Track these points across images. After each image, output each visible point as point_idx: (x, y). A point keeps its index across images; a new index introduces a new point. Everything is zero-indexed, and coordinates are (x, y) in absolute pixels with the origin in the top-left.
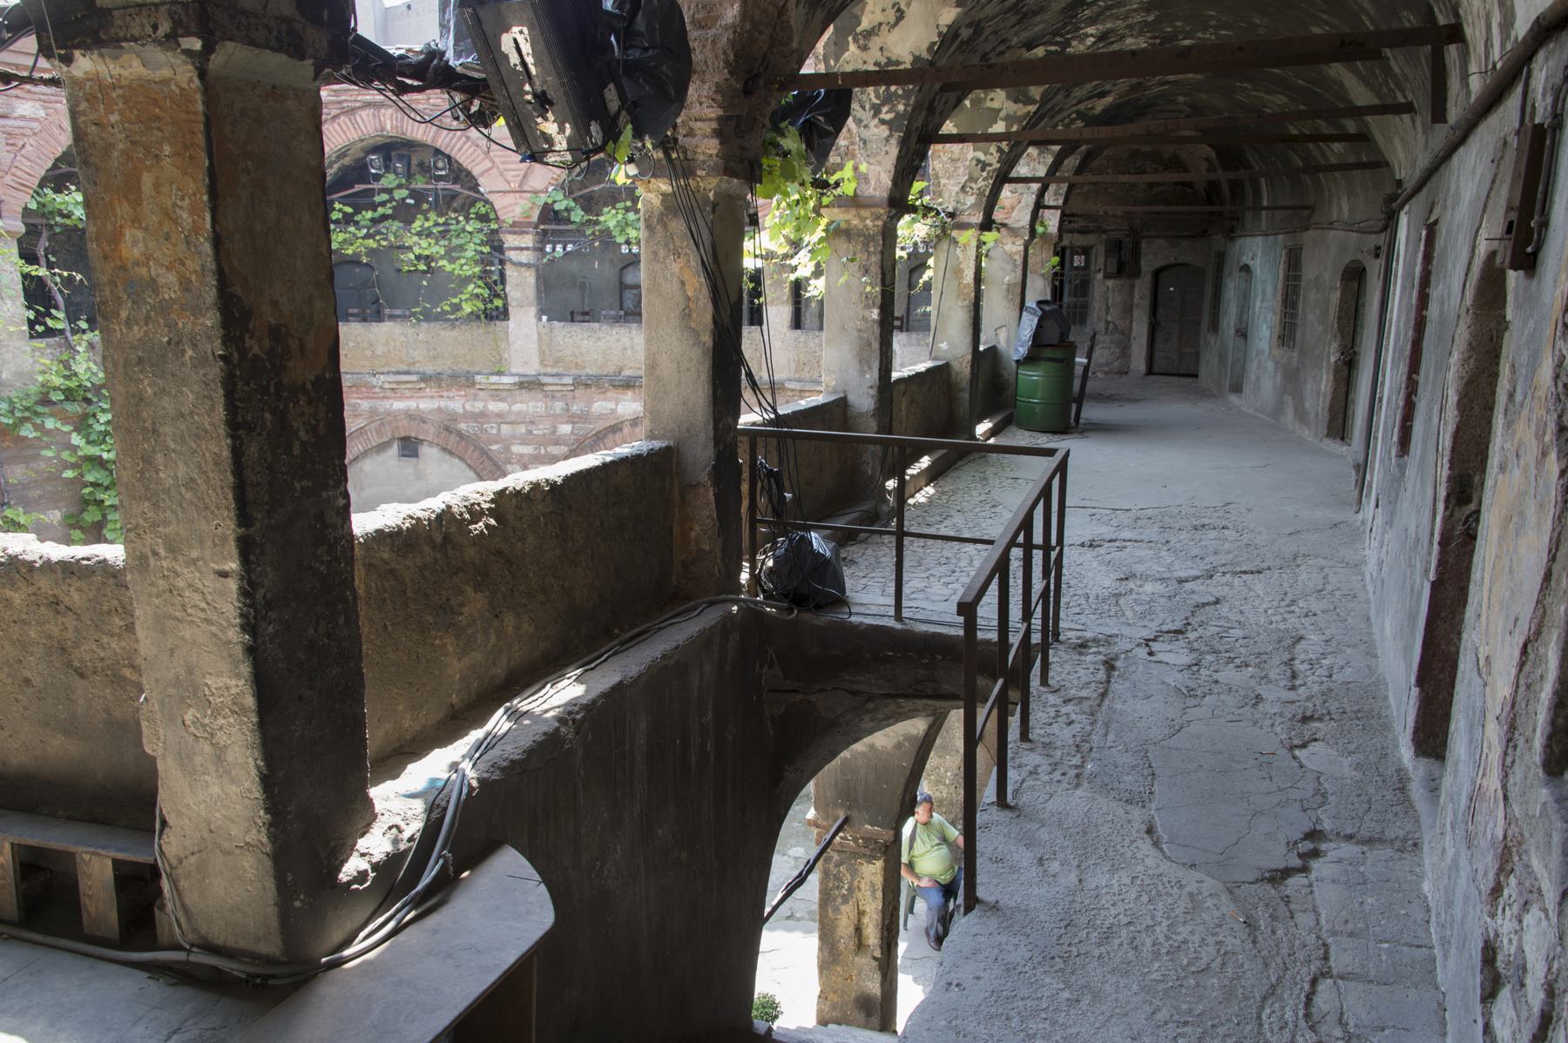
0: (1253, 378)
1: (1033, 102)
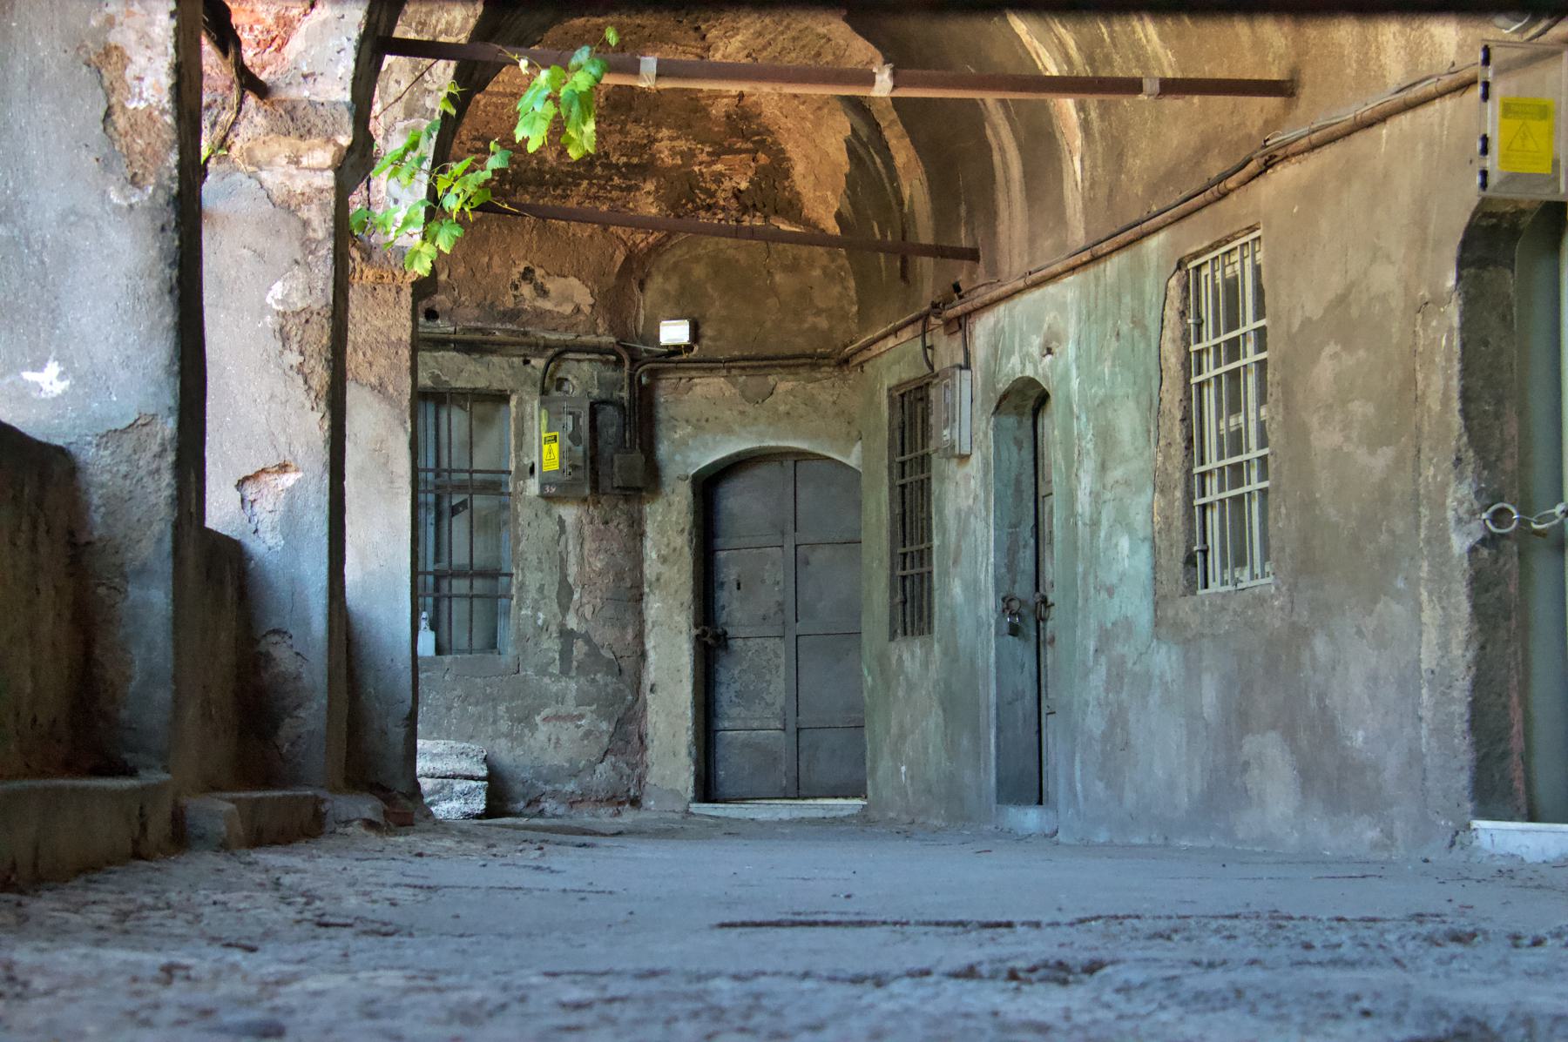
0: (1095, 723)
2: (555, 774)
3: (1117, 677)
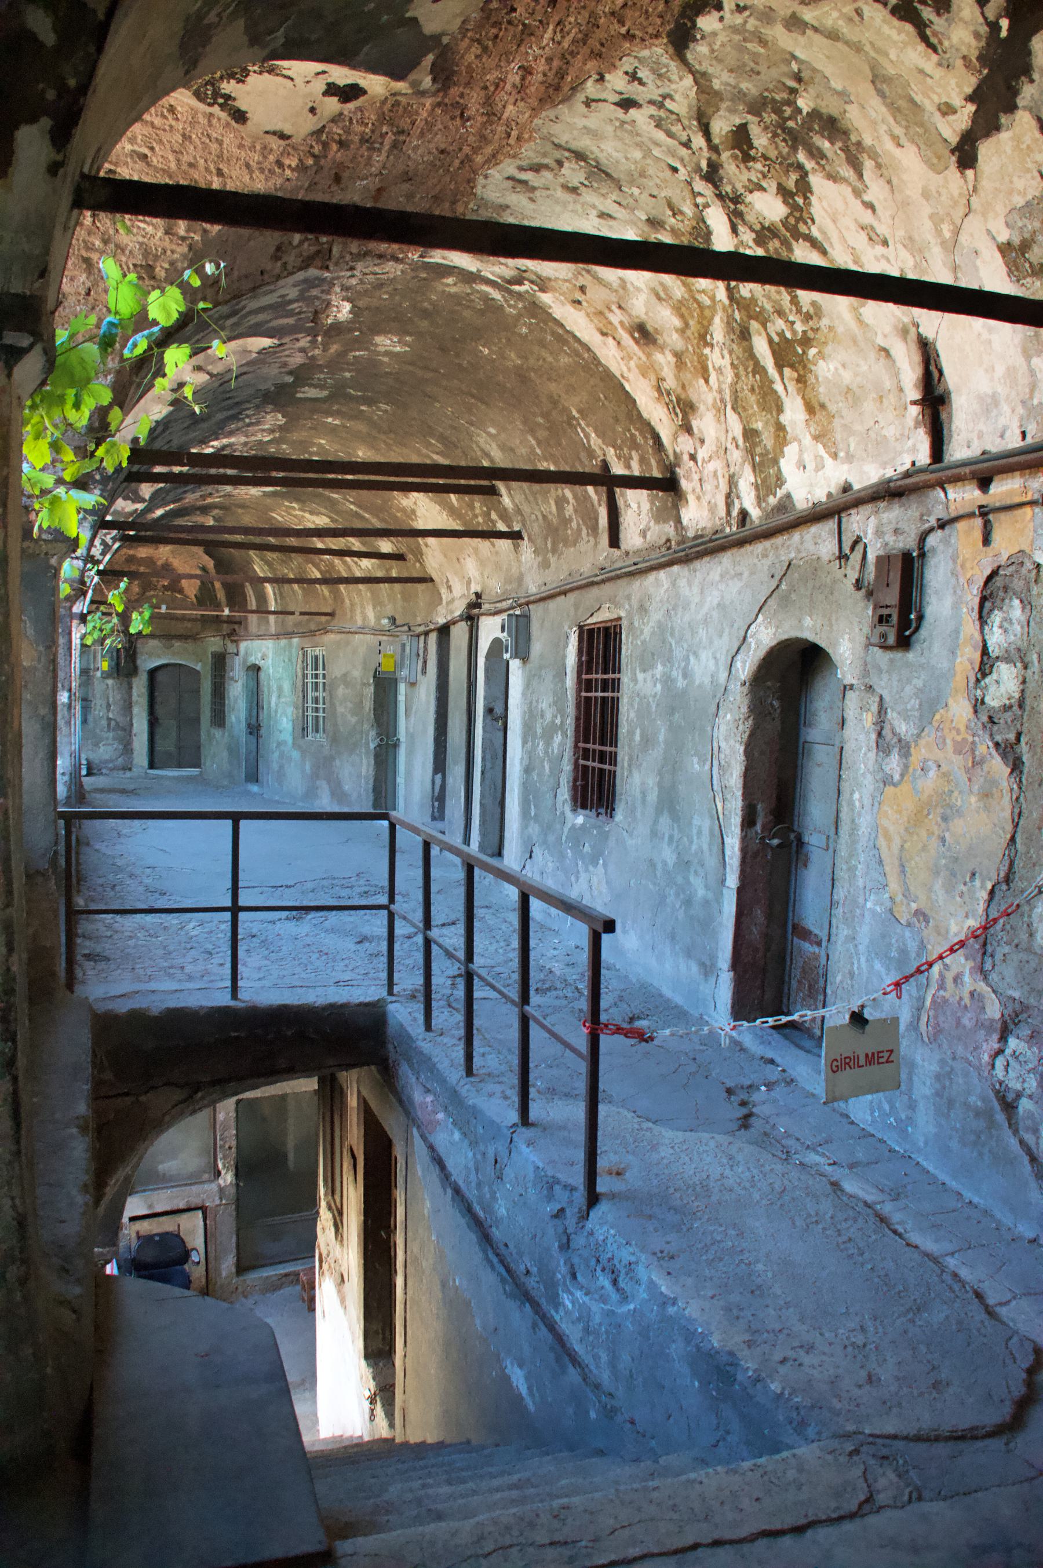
0: (275, 766)
1: (143, 500)
2: (107, 761)
3: (282, 756)
